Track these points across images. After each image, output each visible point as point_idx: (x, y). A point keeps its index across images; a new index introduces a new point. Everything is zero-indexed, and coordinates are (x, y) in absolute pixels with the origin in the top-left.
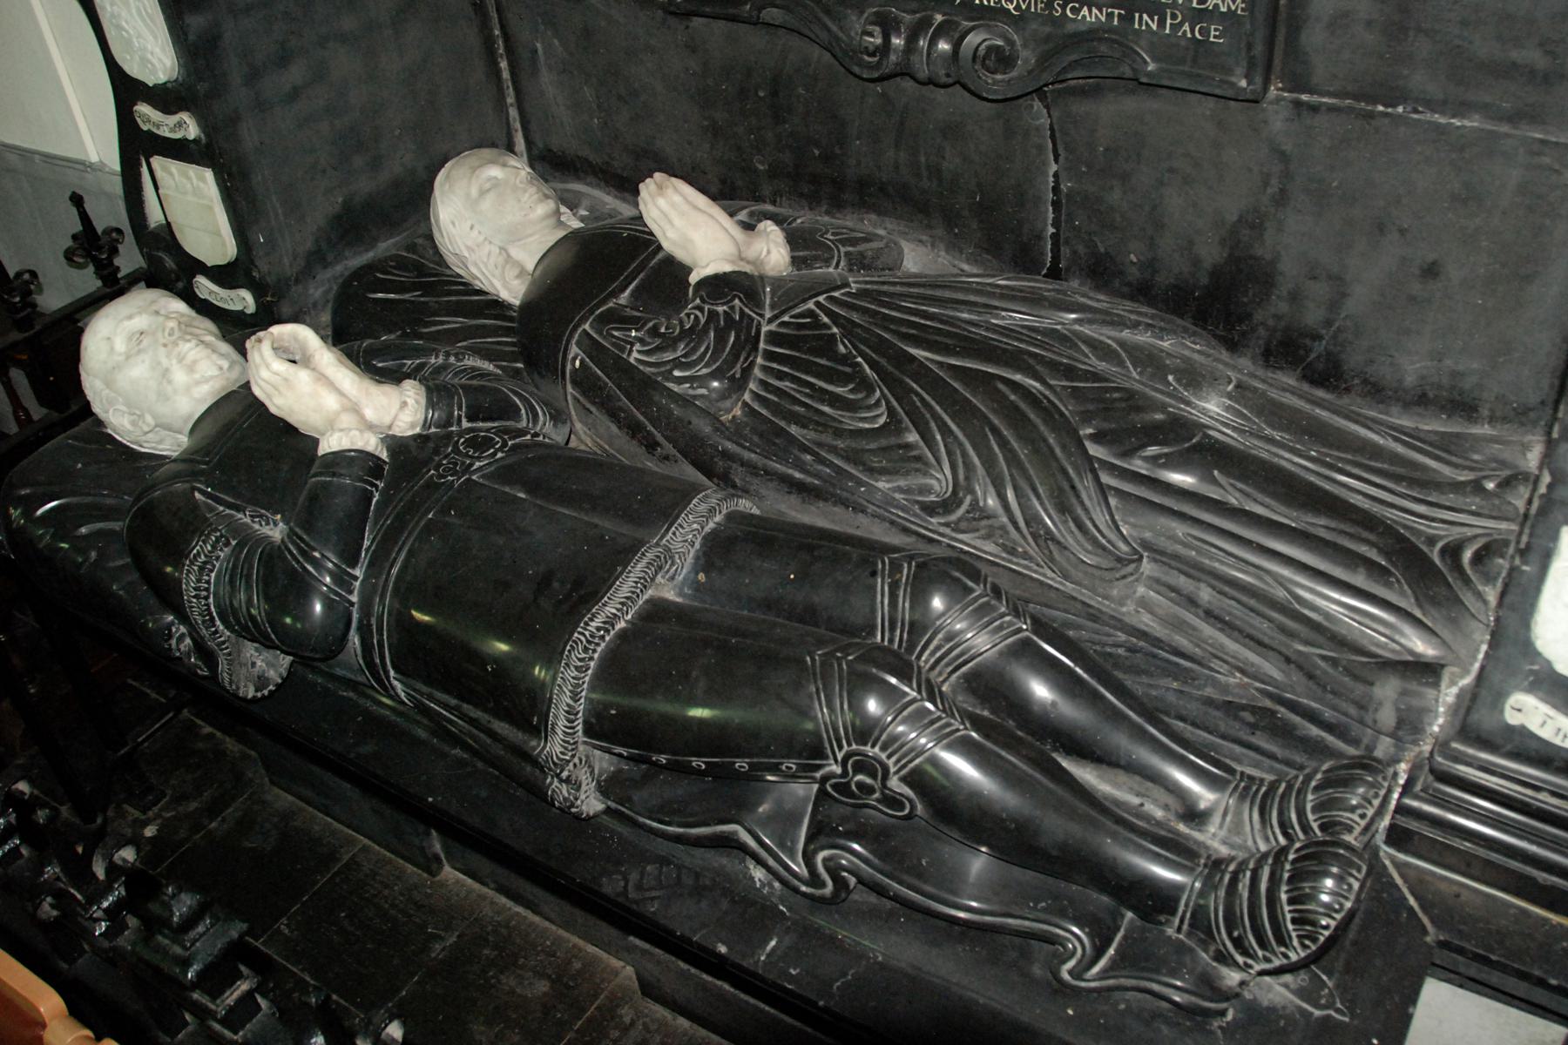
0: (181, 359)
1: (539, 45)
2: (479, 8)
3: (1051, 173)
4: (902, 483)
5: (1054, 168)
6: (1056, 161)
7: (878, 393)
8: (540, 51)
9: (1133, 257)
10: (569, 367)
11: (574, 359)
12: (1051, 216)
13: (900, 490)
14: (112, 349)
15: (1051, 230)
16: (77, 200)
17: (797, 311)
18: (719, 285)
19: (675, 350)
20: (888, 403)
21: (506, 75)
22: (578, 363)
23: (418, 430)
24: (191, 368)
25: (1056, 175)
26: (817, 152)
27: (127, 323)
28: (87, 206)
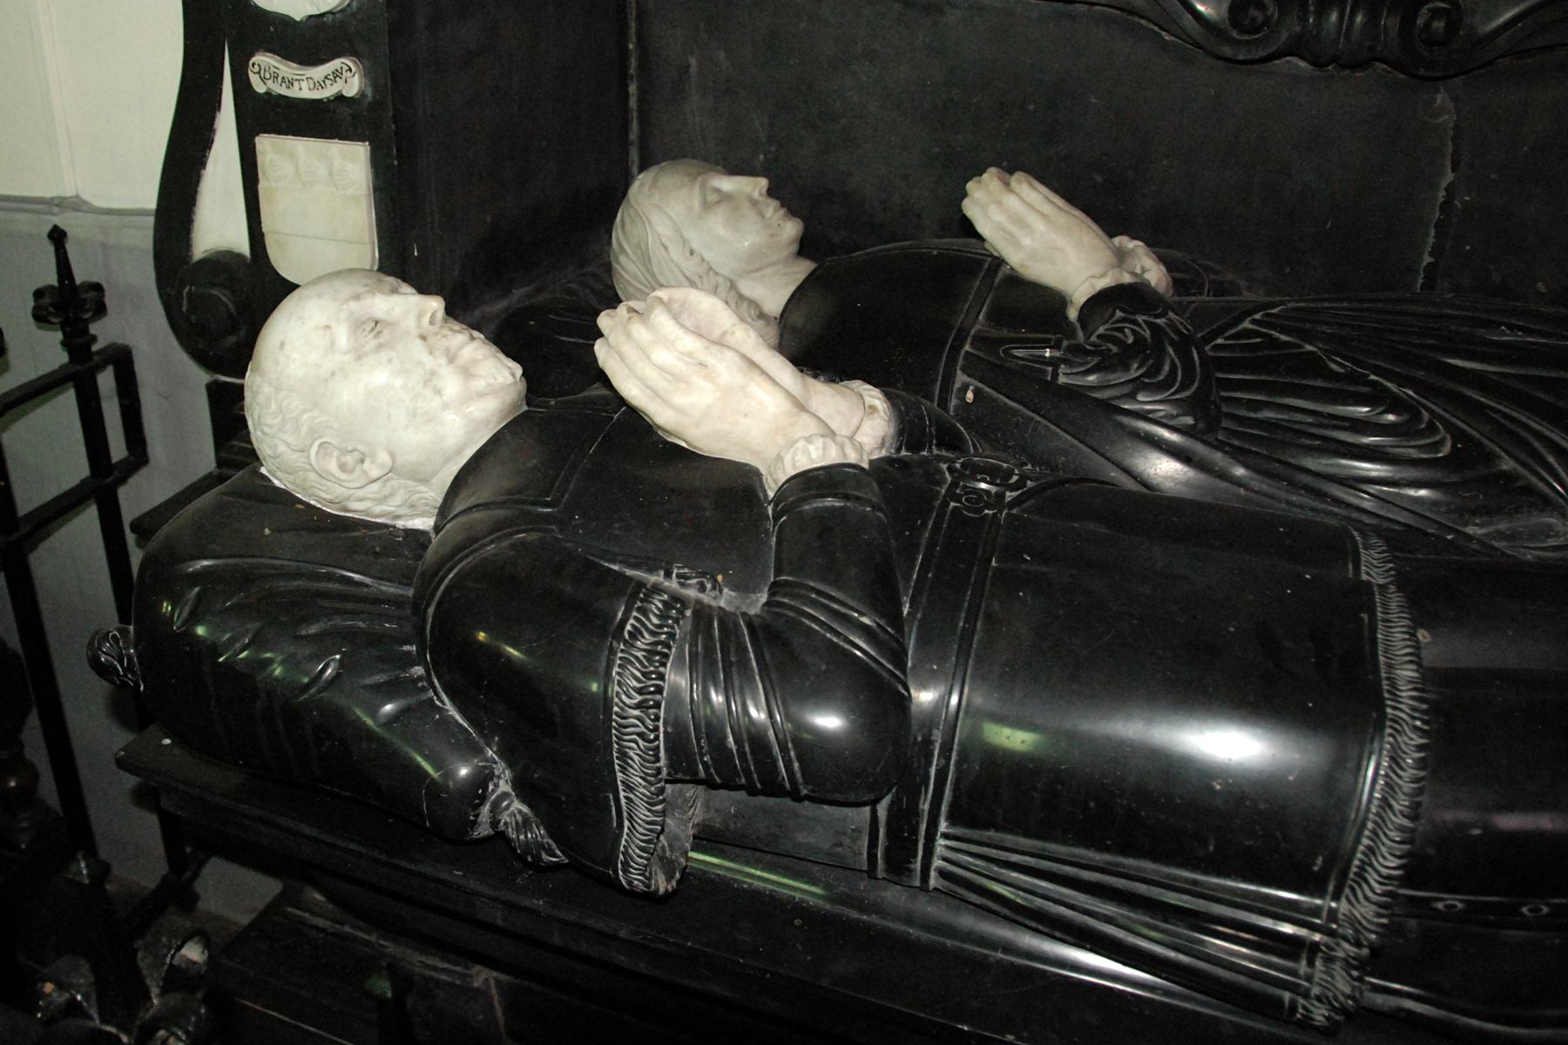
0: (451, 360)
1: (693, 61)
2: (622, 9)
3: (1444, 185)
4: (1502, 526)
5: (1449, 177)
6: (1453, 170)
7: (1426, 415)
8: (694, 69)
9: (1541, 287)
10: (954, 402)
11: (964, 388)
12: (1431, 240)
13: (1500, 535)
14: (333, 343)
15: (1427, 259)
16: (58, 237)
17: (1233, 331)
18: (1102, 301)
19: (1127, 368)
20: (1449, 426)
21: (633, 103)
22: (970, 396)
23: (884, 453)
24: (467, 373)
25: (1449, 188)
26: (1099, 179)
27: (353, 305)
28: (70, 248)
